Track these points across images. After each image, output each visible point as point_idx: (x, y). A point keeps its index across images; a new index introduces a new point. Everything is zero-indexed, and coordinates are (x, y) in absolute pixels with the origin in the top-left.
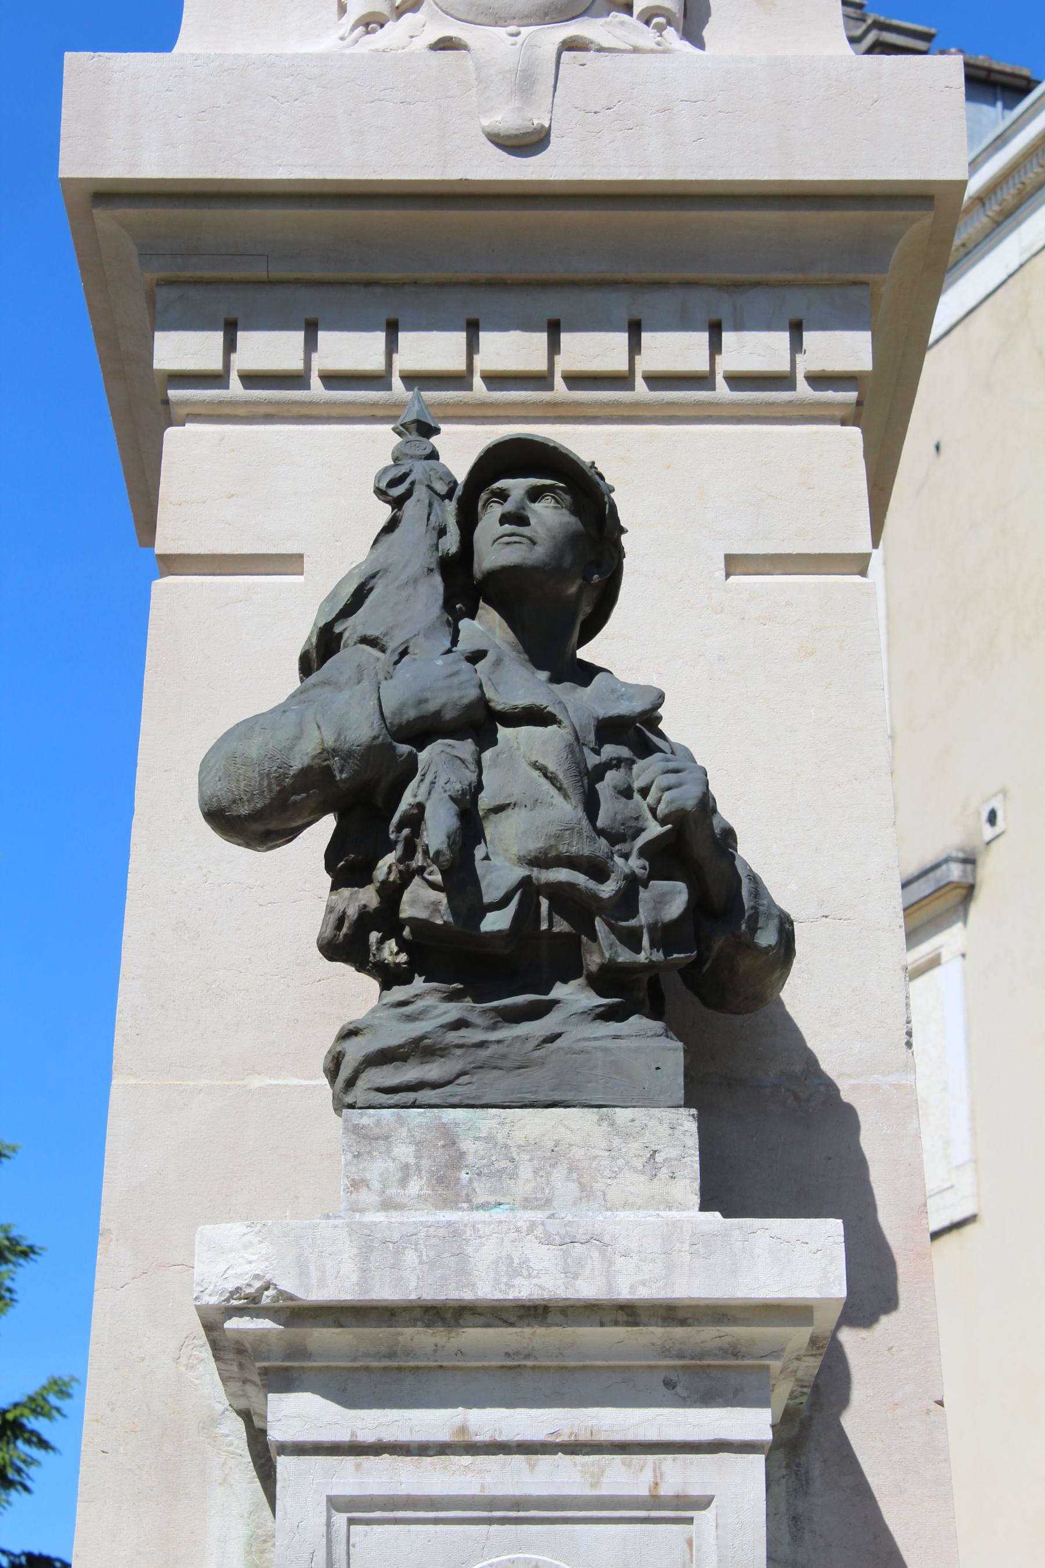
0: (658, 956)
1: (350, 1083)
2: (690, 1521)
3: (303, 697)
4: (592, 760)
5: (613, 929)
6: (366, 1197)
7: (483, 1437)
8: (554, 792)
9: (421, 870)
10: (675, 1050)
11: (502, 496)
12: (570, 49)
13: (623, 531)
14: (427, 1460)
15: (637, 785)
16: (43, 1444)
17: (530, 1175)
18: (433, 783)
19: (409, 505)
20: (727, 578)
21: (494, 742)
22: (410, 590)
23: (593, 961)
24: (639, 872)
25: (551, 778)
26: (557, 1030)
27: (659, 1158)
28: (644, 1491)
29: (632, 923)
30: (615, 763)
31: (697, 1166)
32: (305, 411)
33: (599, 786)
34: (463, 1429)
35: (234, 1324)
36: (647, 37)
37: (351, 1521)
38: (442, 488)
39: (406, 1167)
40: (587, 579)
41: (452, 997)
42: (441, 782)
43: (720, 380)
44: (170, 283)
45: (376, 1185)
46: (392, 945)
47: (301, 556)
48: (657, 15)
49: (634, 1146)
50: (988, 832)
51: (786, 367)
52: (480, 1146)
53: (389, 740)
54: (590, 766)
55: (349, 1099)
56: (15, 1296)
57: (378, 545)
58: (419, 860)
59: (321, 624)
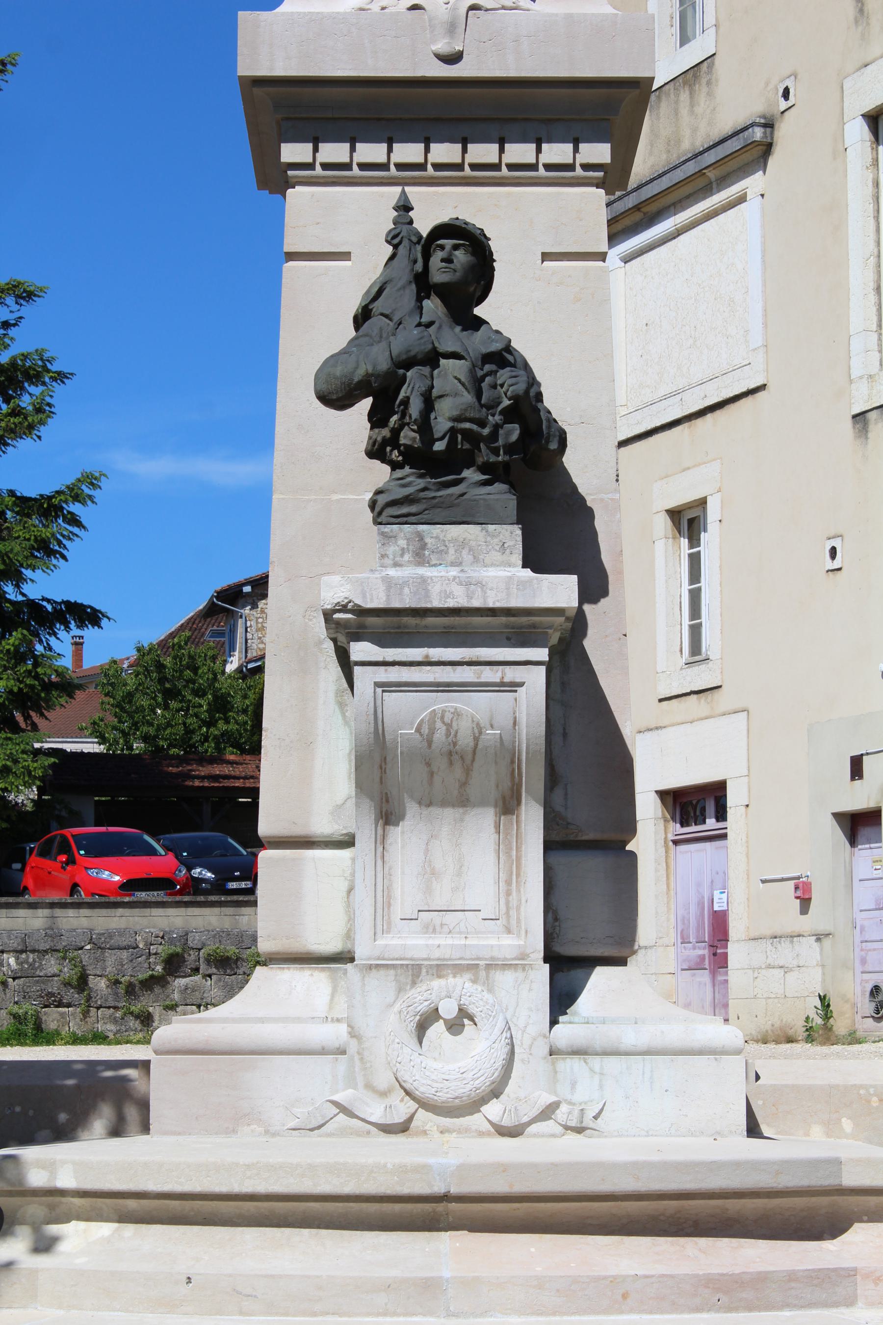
0: (507, 458)
1: (380, 513)
2: (516, 691)
3: (357, 342)
4: (480, 373)
5: (488, 448)
6: (387, 561)
8: (463, 390)
9: (408, 424)
10: (513, 499)
11: (442, 247)
12: (472, 10)
13: (494, 261)
15: (499, 382)
16: (74, 521)
17: (453, 552)
18: (413, 388)
19: (401, 248)
20: (542, 263)
21: (438, 366)
22: (402, 292)
23: (480, 460)
24: (499, 422)
25: (463, 384)
26: (465, 491)
27: (506, 545)
28: (498, 680)
29: (496, 445)
30: (489, 374)
31: (521, 549)
33: (483, 385)
34: (427, 656)
35: (337, 616)
37: (383, 691)
38: (414, 239)
39: (403, 549)
41: (421, 476)
44: (288, 119)
46: (396, 452)
47: (350, 253)
49: (496, 540)
50: (783, 104)
53: (395, 369)
54: (479, 376)
55: (379, 520)
56: (53, 410)
58: (407, 419)
59: (363, 305)
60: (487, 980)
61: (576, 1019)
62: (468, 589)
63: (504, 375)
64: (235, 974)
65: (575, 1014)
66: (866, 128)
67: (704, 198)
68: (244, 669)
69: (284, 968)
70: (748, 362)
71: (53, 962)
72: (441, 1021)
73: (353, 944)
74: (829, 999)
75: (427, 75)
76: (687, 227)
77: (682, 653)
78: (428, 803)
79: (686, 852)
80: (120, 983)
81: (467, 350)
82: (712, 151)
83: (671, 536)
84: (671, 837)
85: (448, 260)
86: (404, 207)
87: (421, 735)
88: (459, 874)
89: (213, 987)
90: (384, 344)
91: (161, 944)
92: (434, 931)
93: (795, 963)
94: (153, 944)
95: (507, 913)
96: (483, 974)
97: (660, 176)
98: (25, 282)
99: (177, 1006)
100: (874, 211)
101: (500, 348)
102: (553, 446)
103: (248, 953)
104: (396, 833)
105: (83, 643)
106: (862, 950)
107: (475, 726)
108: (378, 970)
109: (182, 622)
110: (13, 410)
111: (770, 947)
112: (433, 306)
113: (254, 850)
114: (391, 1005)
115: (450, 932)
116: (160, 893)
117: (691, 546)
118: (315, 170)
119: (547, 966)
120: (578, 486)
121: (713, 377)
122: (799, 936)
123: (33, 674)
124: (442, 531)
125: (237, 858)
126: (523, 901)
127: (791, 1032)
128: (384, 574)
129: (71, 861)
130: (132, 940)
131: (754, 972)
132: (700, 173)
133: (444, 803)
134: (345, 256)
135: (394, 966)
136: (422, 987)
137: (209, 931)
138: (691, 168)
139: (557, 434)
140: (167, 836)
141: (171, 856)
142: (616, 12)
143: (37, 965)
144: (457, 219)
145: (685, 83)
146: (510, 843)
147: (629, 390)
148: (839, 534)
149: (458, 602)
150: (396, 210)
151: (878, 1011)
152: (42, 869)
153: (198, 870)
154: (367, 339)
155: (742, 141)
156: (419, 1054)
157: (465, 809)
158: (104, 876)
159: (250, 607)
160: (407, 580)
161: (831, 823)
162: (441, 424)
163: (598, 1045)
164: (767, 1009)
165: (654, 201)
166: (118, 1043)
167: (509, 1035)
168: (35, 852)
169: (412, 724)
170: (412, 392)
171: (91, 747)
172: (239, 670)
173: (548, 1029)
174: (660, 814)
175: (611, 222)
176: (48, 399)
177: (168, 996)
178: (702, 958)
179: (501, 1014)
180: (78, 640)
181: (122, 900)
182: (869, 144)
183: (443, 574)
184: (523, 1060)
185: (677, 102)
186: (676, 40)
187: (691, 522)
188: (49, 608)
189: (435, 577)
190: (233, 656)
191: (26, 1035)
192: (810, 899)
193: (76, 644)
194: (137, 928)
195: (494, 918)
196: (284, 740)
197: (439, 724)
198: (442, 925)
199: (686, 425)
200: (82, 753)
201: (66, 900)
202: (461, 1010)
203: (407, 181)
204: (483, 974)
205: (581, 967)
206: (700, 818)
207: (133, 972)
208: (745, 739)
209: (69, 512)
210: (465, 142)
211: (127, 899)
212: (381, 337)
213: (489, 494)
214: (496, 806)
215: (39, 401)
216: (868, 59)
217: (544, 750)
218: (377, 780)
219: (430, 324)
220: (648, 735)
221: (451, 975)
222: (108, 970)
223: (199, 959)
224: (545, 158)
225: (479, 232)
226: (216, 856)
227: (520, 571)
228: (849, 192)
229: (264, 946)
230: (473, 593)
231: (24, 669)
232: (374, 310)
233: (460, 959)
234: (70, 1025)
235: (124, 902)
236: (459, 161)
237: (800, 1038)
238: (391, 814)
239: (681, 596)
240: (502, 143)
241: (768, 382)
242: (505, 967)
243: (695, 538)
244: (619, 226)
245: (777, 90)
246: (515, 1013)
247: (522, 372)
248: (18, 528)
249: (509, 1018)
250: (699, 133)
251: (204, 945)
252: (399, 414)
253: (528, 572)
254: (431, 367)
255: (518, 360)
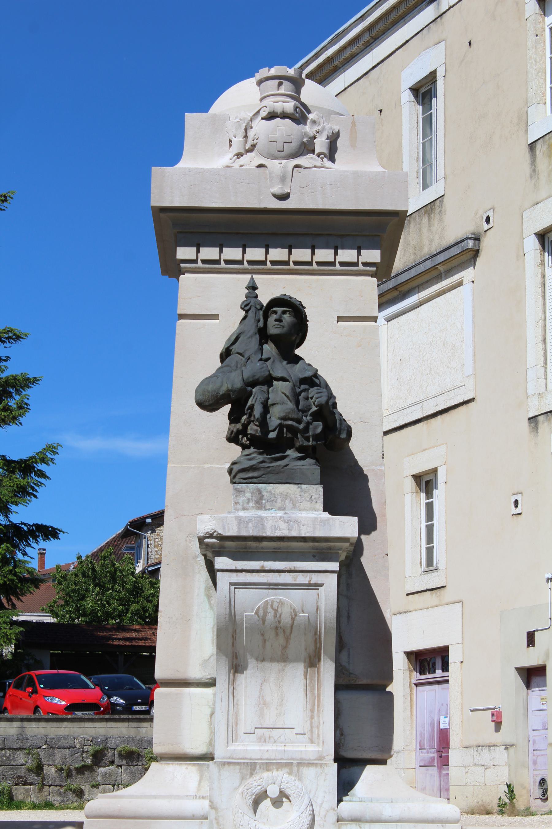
0: (314, 443)
1: (235, 477)
2: (318, 589)
3: (222, 370)
4: (298, 390)
5: (303, 436)
7: (268, 568)
8: (288, 400)
9: (253, 421)
10: (318, 469)
11: (276, 312)
13: (308, 321)
14: (254, 574)
15: (310, 396)
16: (42, 474)
17: (280, 501)
18: (256, 399)
19: (250, 312)
20: (338, 323)
21: (272, 385)
23: (297, 444)
24: (310, 420)
25: (288, 397)
26: (288, 463)
27: (313, 498)
28: (307, 582)
29: (308, 435)
31: (323, 500)
32: (219, 270)
34: (263, 567)
35: (207, 540)
36: (318, 162)
37: (235, 588)
38: (258, 307)
39: (249, 499)
40: (298, 335)
41: (261, 454)
42: (259, 398)
43: (337, 264)
44: (181, 232)
45: (241, 504)
46: (245, 439)
47: (218, 315)
48: (322, 154)
49: (307, 494)
50: (486, 227)
51: (356, 261)
52: (267, 494)
54: (297, 392)
55: (234, 481)
56: (29, 407)
57: (241, 323)
58: (252, 418)
59: (226, 347)
60: (298, 773)
61: (354, 799)
62: (289, 525)
63: (313, 391)
64: (137, 765)
65: (353, 795)
66: (537, 242)
67: (437, 283)
68: (146, 571)
69: (169, 763)
70: (463, 384)
71: (21, 756)
72: (269, 799)
73: (214, 749)
74: (513, 787)
75: (267, 207)
76: (426, 300)
77: (421, 565)
78: (262, 659)
79: (424, 691)
80: (63, 770)
81: (290, 376)
82: (442, 254)
83: (415, 492)
84: (413, 681)
85: (279, 320)
86: (252, 287)
87: (258, 616)
88: (281, 705)
89: (123, 773)
90: (239, 371)
91: (90, 745)
92: (265, 741)
93: (492, 763)
94: (85, 746)
95: (311, 730)
96: (295, 769)
97: (410, 269)
98: (15, 329)
99: (99, 785)
100: (542, 292)
101: (311, 375)
102: (343, 436)
103: (145, 751)
104: (242, 678)
105: (46, 553)
106: (534, 755)
107: (292, 611)
108: (229, 766)
109: (108, 540)
110: (4, 407)
111: (476, 753)
112: (269, 348)
113: (150, 686)
114: (236, 788)
115: (275, 742)
116: (90, 712)
117: (428, 498)
118: (197, 264)
119: (336, 764)
120: (358, 461)
121: (442, 393)
122: (494, 746)
123: (13, 572)
124: (273, 488)
125: (139, 690)
126: (321, 722)
127: (489, 808)
128: (236, 514)
129: (35, 691)
130: (72, 742)
131: (465, 768)
132: (435, 267)
133: (272, 660)
134: (215, 317)
135: (239, 763)
136: (257, 777)
137: (121, 737)
138: (429, 264)
139: (346, 428)
140: (96, 676)
141: (98, 690)
142: (385, 170)
143: (12, 758)
144: (285, 295)
145: (425, 212)
146: (314, 686)
147: (389, 400)
148: (520, 492)
149: (283, 533)
150: (247, 289)
151: (544, 795)
152: (17, 696)
153: (115, 698)
154: (228, 368)
155: (460, 248)
156: (254, 820)
157: (285, 663)
158: (55, 701)
159: (150, 532)
160: (251, 518)
161: (515, 674)
162: (274, 421)
163: (368, 816)
164: (473, 793)
165: (405, 284)
166: (62, 809)
167: (311, 809)
168: (13, 684)
169: (253, 609)
170: (256, 401)
171: (48, 619)
172: (143, 572)
173: (336, 805)
174: (407, 667)
175: (380, 296)
176: (26, 401)
177: (94, 779)
178: (433, 759)
179: (307, 795)
180: (42, 551)
181: (66, 717)
182: (539, 251)
183: (273, 515)
184: (320, 825)
185: (420, 224)
186: (420, 186)
187: (427, 483)
188: (25, 528)
189: (269, 517)
190: (139, 562)
191: (3, 803)
192: (501, 722)
193: (41, 554)
194: (76, 735)
195: (303, 733)
196: (172, 618)
197: (270, 609)
198: (270, 737)
199: (425, 422)
200: (43, 622)
201: (31, 716)
202: (281, 792)
203: (255, 271)
204: (295, 769)
205: (357, 765)
206: (432, 670)
207: (72, 763)
208: (461, 619)
209: (38, 469)
210: (290, 248)
211: (69, 716)
212: (237, 367)
213: (303, 465)
214: (305, 662)
215: (20, 402)
216: (538, 200)
217: (335, 627)
218: (231, 644)
219: (267, 360)
220: (400, 616)
221: (275, 770)
222: (56, 761)
223: (114, 755)
224: (340, 258)
225: (299, 303)
226: (126, 689)
227: (322, 514)
228: (526, 281)
229: (157, 749)
230: (292, 527)
231: (8, 569)
232: (233, 350)
233: (281, 759)
234: (32, 797)
235: (67, 718)
236: (287, 259)
237: (494, 812)
238: (239, 666)
239: (421, 529)
240: (313, 249)
241: (476, 396)
242: (309, 765)
243: (430, 493)
244: (384, 299)
245: (482, 217)
246: (315, 794)
247: (324, 390)
248: (6, 480)
249: (311, 797)
250: (434, 243)
251: (117, 746)
252: (248, 415)
253: (327, 515)
254: (268, 386)
255: (322, 382)
